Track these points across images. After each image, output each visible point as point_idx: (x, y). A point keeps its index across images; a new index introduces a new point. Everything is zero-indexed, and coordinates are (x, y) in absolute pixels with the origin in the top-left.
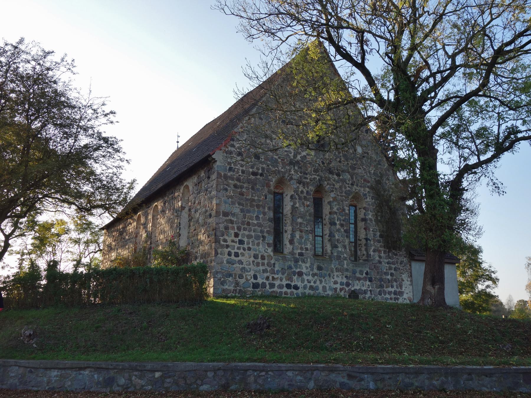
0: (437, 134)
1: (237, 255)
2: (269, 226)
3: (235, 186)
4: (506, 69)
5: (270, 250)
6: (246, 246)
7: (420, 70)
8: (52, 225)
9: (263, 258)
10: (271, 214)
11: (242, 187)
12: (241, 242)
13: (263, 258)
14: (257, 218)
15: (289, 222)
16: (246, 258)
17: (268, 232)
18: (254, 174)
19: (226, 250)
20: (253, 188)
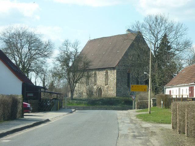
0: (53, 57)
1: (120, 88)
2: (126, 81)
3: (120, 73)
4: (155, 44)
5: (127, 87)
6: (122, 86)
7: (17, 64)
8: (102, 104)
9: (125, 88)
10: (127, 79)
11: (121, 73)
12: (121, 85)
13: (125, 88)
14: (124, 80)
15: (131, 80)
16: (122, 88)
17: (127, 83)
18: (124, 70)
19: (118, 87)
20: (123, 73)
